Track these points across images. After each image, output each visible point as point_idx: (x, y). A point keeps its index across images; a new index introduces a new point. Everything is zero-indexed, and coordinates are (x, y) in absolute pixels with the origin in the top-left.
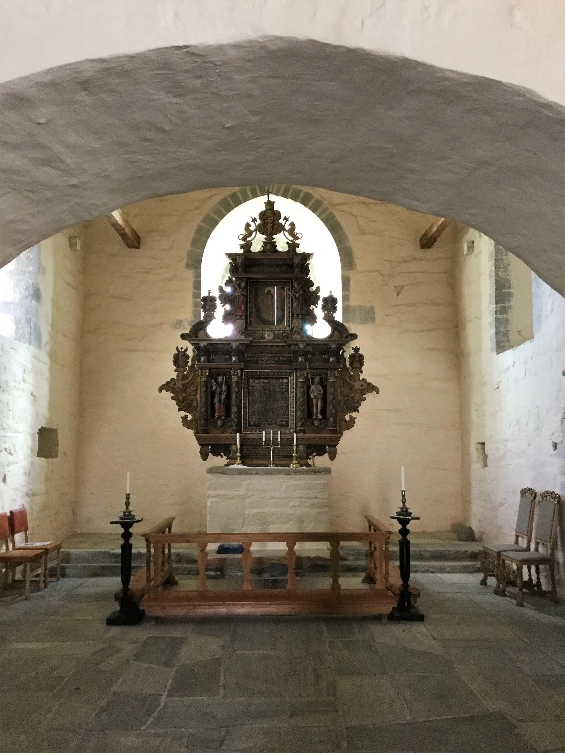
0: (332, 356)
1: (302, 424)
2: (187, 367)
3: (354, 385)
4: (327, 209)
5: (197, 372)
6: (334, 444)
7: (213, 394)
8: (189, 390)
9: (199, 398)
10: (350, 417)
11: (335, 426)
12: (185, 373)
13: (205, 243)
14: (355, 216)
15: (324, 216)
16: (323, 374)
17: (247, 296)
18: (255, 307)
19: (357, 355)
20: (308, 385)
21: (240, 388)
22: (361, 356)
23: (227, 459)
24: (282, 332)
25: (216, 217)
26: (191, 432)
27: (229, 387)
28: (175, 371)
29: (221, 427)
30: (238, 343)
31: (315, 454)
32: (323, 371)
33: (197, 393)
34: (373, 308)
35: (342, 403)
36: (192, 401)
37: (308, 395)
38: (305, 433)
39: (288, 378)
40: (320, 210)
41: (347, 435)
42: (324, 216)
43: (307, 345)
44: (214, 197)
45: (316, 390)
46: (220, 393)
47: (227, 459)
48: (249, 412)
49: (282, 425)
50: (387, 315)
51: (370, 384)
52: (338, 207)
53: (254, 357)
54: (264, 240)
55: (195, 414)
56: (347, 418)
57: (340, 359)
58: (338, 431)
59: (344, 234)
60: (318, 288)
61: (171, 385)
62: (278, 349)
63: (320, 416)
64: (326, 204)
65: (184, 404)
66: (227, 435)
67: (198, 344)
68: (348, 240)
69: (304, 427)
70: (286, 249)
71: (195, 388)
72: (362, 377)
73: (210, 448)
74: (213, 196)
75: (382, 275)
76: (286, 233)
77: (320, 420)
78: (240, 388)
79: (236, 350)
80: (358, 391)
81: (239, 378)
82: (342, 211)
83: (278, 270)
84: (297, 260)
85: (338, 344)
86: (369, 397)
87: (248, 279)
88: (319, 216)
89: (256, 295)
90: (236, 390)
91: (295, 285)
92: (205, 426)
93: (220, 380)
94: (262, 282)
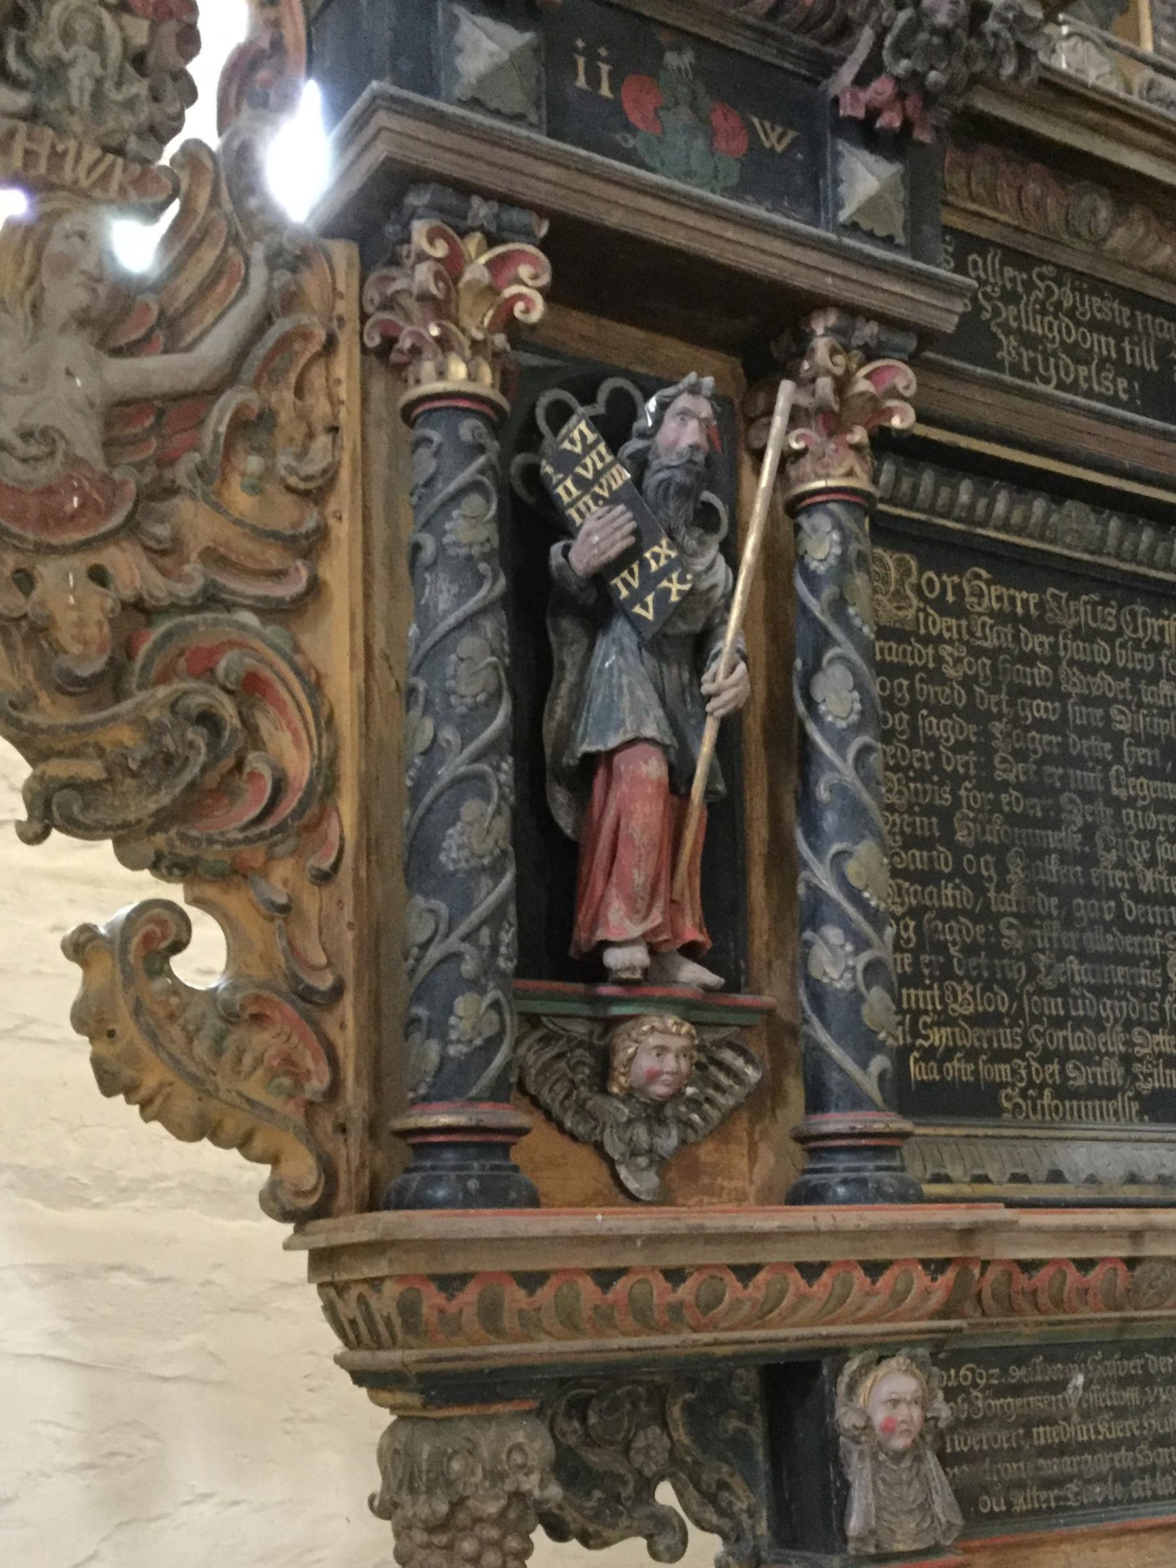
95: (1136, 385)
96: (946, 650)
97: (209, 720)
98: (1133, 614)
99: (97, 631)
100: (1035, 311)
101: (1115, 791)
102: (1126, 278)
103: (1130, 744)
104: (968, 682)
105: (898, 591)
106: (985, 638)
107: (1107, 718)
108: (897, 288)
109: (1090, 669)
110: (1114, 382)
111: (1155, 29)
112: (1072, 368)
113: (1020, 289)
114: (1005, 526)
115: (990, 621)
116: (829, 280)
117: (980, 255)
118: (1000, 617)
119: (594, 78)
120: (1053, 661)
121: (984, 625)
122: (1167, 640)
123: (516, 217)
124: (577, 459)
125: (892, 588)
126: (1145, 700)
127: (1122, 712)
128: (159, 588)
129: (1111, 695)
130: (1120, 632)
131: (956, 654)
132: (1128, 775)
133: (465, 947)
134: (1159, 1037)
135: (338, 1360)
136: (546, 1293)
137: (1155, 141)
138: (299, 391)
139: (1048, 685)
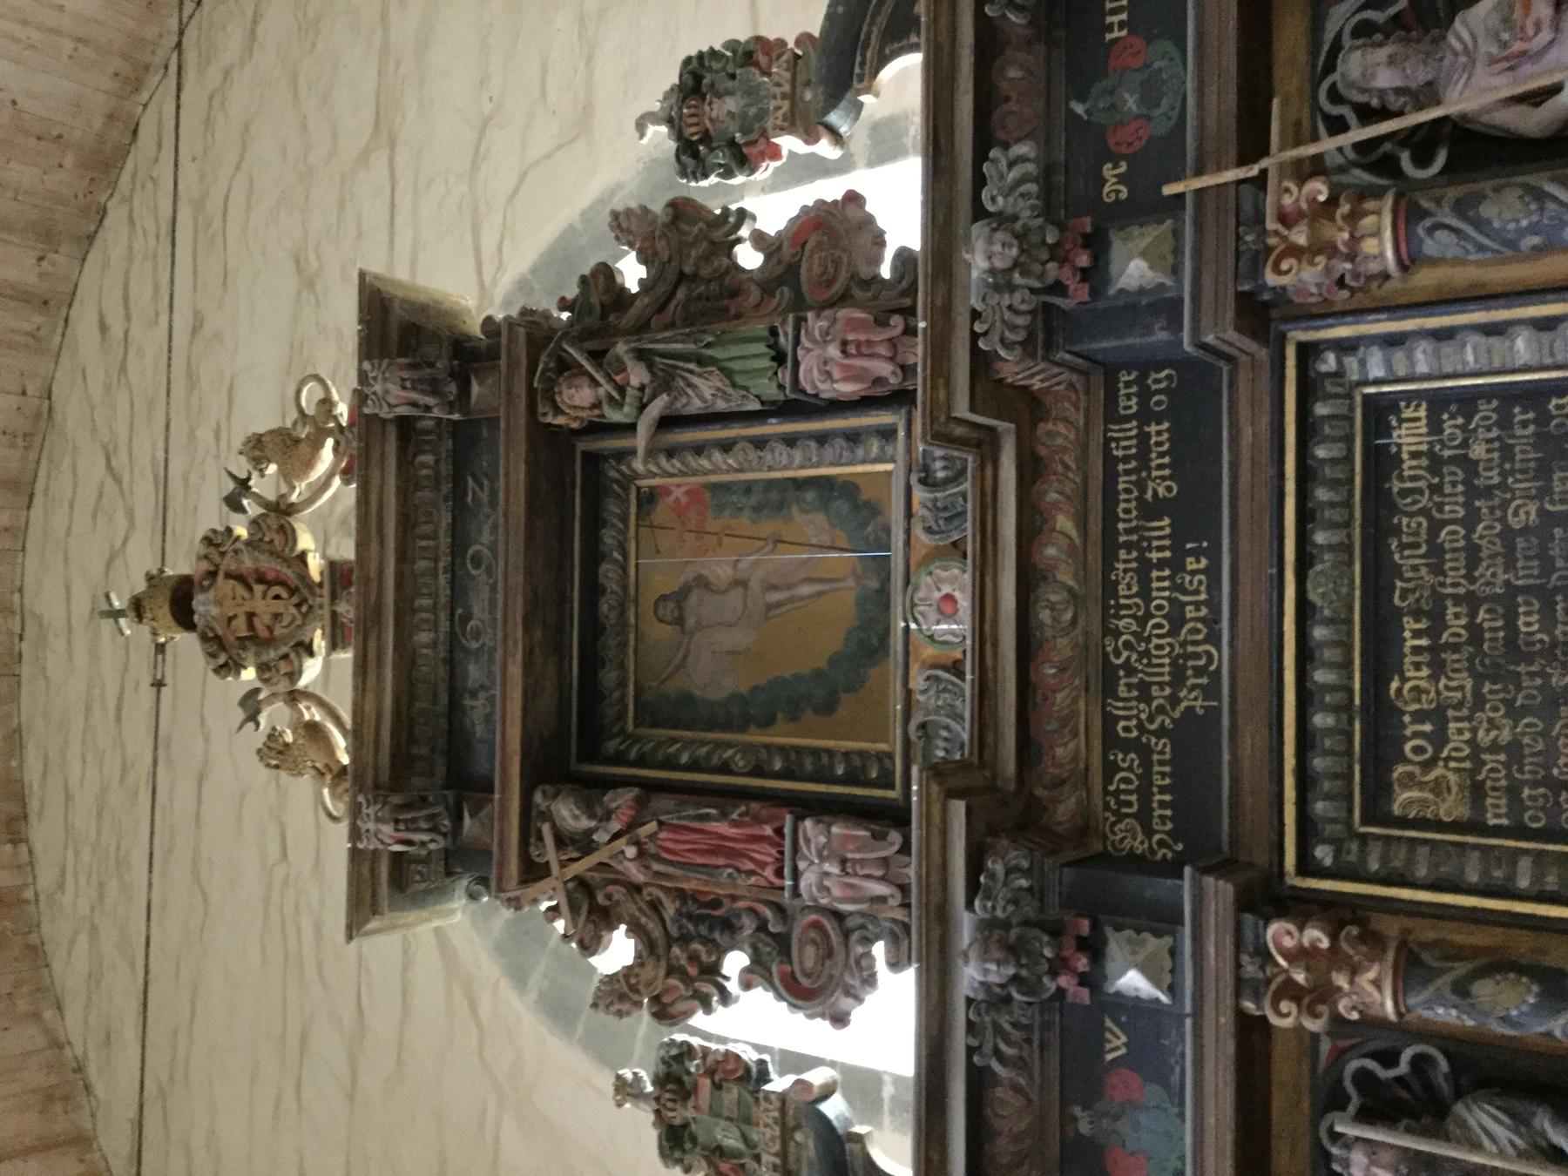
17: (651, 788)
18: (767, 722)
24: (919, 494)
39: (1380, 413)
53: (1145, 753)
62: (1064, 523)
79: (1014, 951)
89: (683, 711)
91: (578, 398)
95: (1189, 546)
98: (1404, 493)
100: (1150, 665)
102: (1095, 557)
103: (1552, 502)
104: (1515, 713)
105: (1432, 791)
106: (1462, 688)
107: (1525, 531)
108: (1211, 950)
109: (1473, 555)
110: (1194, 573)
111: (863, 462)
112: (1190, 625)
113: (1134, 680)
114: (1347, 665)
115: (1443, 681)
116: (1223, 1020)
117: (1117, 724)
118: (1438, 668)
120: (1471, 601)
121: (1447, 688)
122: (1424, 448)
125: (1431, 796)
126: (1496, 480)
127: (1516, 514)
129: (1499, 527)
131: (1485, 725)
137: (988, 580)
139: (1501, 610)
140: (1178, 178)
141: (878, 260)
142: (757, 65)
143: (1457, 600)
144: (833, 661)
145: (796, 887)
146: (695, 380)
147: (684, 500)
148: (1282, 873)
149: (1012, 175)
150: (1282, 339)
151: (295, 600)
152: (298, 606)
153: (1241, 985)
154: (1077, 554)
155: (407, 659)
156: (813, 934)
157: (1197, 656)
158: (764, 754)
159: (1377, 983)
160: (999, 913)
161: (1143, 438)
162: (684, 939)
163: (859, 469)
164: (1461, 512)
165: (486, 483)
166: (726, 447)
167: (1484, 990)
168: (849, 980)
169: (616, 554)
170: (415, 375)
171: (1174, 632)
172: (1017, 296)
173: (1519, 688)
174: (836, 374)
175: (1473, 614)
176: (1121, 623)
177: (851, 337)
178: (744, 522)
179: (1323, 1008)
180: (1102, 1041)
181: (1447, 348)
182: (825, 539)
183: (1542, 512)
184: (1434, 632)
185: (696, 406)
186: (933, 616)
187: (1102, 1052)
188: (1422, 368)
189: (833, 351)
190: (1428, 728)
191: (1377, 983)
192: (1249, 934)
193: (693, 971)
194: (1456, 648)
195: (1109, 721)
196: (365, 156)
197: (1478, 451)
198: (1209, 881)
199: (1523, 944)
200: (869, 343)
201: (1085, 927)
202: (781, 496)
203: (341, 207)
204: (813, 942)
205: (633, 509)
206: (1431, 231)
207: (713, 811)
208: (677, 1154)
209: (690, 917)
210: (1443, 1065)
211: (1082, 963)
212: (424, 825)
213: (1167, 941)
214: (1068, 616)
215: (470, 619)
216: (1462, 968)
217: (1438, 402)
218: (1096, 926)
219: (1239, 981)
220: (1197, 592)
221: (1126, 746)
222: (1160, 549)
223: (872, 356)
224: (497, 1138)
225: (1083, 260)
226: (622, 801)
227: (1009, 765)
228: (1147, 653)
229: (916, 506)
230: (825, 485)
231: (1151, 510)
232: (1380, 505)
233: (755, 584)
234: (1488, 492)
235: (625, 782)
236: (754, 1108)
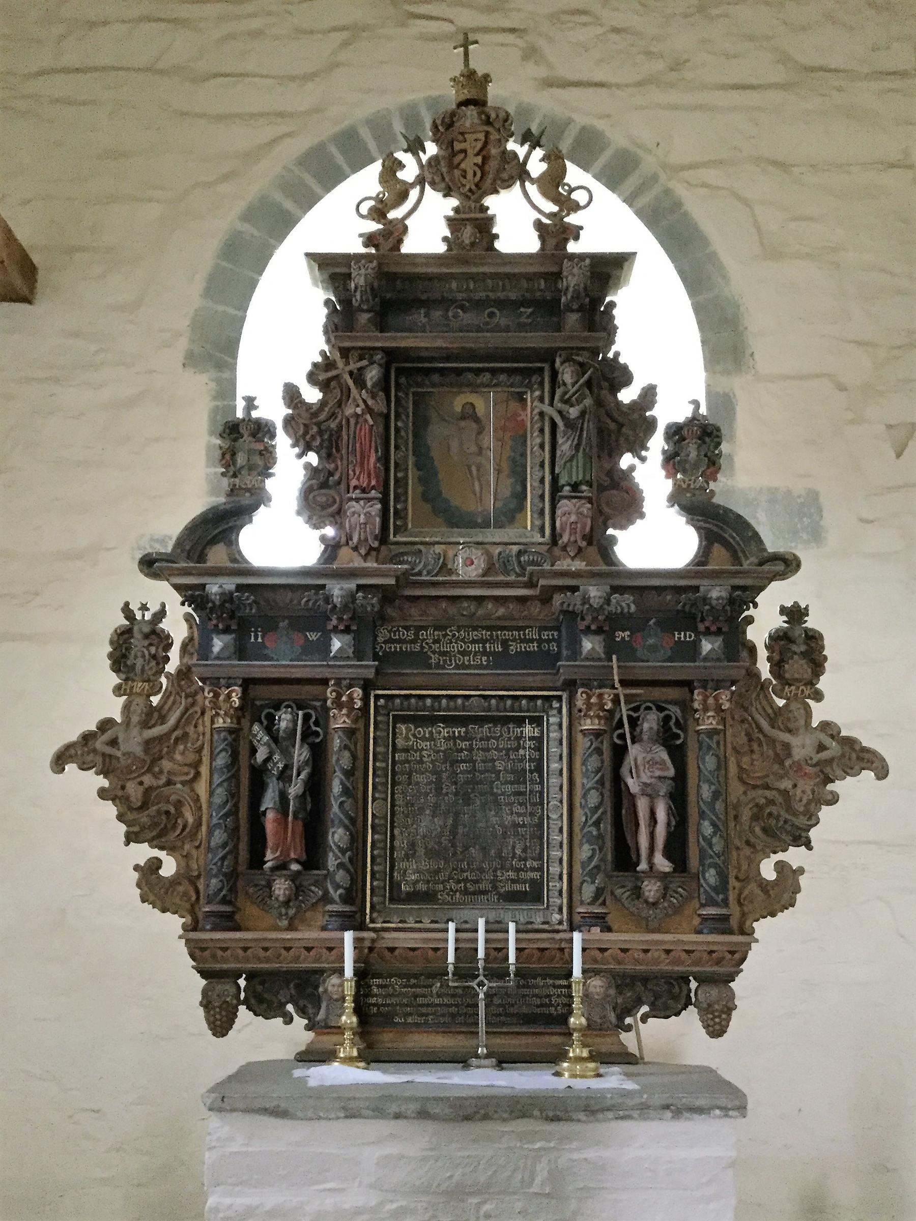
0: (708, 632)
1: (599, 893)
2: (163, 680)
3: (787, 746)
4: (654, 178)
5: (199, 698)
6: (721, 972)
7: (258, 777)
8: (166, 765)
9: (208, 794)
10: (781, 867)
11: (725, 903)
12: (155, 700)
13: (252, 285)
14: (745, 202)
15: (645, 199)
16: (675, 703)
17: (387, 417)
18: (418, 466)
19: (797, 632)
20: (615, 747)
21: (360, 754)
22: (814, 639)
23: (308, 1028)
24: (515, 548)
25: (288, 205)
26: (174, 923)
27: (319, 753)
28: (118, 690)
29: (286, 904)
30: (351, 585)
31: (645, 1009)
32: (674, 693)
33: (198, 774)
34: (813, 497)
35: (746, 814)
36: (179, 804)
37: (617, 781)
38: (609, 929)
40: (632, 182)
41: (772, 937)
42: (645, 199)
43: (615, 589)
44: (288, 140)
45: (646, 765)
46: (285, 776)
47: (308, 1028)
48: (392, 848)
49: (514, 897)
50: (862, 520)
51: (850, 742)
52: (691, 172)
53: (413, 642)
54: (451, 213)
55: (187, 857)
56: (768, 870)
57: (737, 646)
58: (734, 923)
59: (713, 257)
60: (649, 395)
61: (99, 744)
62: (501, 611)
63: (662, 864)
64: (649, 164)
65: (147, 818)
66: (308, 934)
67: (203, 586)
68: (725, 277)
69: (604, 904)
70: (531, 244)
71: (191, 757)
72: (819, 712)
73: (238, 986)
74: (281, 137)
75: (842, 388)
76: (532, 189)
77: (664, 877)
78: (360, 754)
79: (345, 606)
80: (809, 770)
81: (355, 721)
82: (704, 185)
83: (501, 319)
84: (573, 279)
85: (735, 588)
86: (854, 790)
87: (392, 355)
88: (629, 200)
89: (421, 423)
90: (345, 760)
91: (567, 375)
92: (224, 901)
93: (283, 725)
94: (441, 371)
96: (424, 753)
97: (167, 813)
98: (509, 729)
99: (140, 796)
101: (495, 790)
102: (488, 623)
104: (432, 762)
118: (447, 739)
119: (256, 637)
120: (470, 749)
123: (232, 681)
124: (256, 735)
128: (155, 783)
130: (501, 735)
132: (502, 784)
133: (214, 867)
134: (510, 873)
135: (193, 967)
136: (229, 952)
138: (196, 727)
140: (618, 660)
141: (615, 528)
142: (708, 467)
143: (471, 745)
144: (447, 501)
145: (351, 499)
146: (569, 442)
147: (519, 419)
148: (375, 690)
149: (624, 604)
150: (563, 690)
151: (473, 187)
152: (470, 190)
153: (339, 681)
154: (487, 616)
155: (441, 278)
156: (331, 500)
157: (451, 661)
158: (403, 467)
159: (344, 722)
160: (358, 601)
161: (532, 641)
162: (321, 432)
163: (529, 513)
164: (501, 746)
165: (530, 320)
166: (542, 446)
167: (347, 754)
168: (314, 518)
169: (495, 381)
170: (581, 290)
171: (459, 652)
172: (580, 607)
173: (442, 763)
174: (564, 519)
175: (466, 750)
176: (462, 633)
177: (579, 525)
178: (508, 452)
179: (335, 706)
180: (312, 631)
181: (557, 743)
182: (499, 496)
183: (501, 771)
184: (460, 737)
185: (560, 440)
186: (465, 556)
187: (310, 631)
188: (551, 735)
189: (573, 518)
190: (427, 736)
191: (344, 722)
192: (356, 682)
193: (308, 437)
194: (455, 744)
195: (425, 628)
196: (784, 59)
197: (521, 752)
198: (373, 670)
199: (360, 763)
200: (576, 533)
201: (354, 628)
202: (518, 472)
203: (751, 38)
204: (328, 500)
205: (517, 390)
206: (591, 740)
207: (380, 453)
208: (227, 431)
209: (331, 435)
210: (318, 740)
211: (341, 627)
212: (364, 298)
213: (351, 655)
214: (465, 613)
215: (464, 312)
216: (352, 747)
217: (539, 740)
218: (354, 631)
219: (340, 679)
220: (474, 661)
221: (416, 635)
222: (490, 647)
223: (571, 535)
224: (150, 200)
225: (593, 627)
226: (379, 405)
227: (407, 592)
228: (451, 643)
229: (511, 547)
230: (521, 497)
231: (505, 643)
232: (505, 721)
233: (479, 459)
234: (507, 754)
235: (389, 405)
236: (256, 473)
